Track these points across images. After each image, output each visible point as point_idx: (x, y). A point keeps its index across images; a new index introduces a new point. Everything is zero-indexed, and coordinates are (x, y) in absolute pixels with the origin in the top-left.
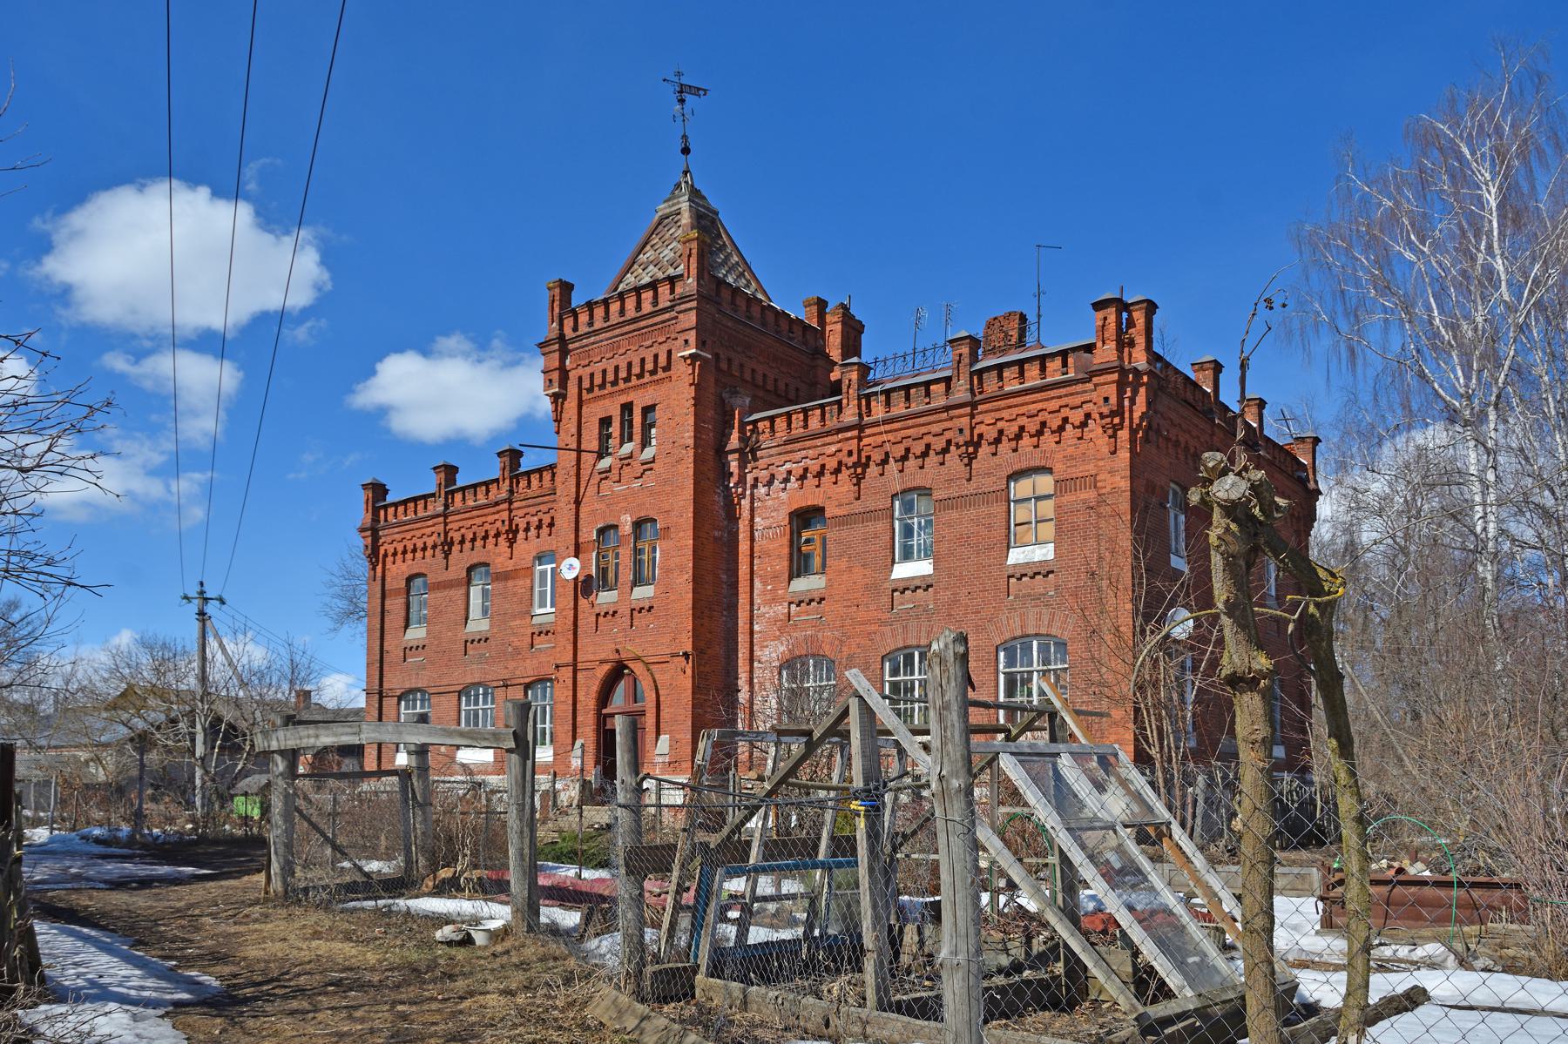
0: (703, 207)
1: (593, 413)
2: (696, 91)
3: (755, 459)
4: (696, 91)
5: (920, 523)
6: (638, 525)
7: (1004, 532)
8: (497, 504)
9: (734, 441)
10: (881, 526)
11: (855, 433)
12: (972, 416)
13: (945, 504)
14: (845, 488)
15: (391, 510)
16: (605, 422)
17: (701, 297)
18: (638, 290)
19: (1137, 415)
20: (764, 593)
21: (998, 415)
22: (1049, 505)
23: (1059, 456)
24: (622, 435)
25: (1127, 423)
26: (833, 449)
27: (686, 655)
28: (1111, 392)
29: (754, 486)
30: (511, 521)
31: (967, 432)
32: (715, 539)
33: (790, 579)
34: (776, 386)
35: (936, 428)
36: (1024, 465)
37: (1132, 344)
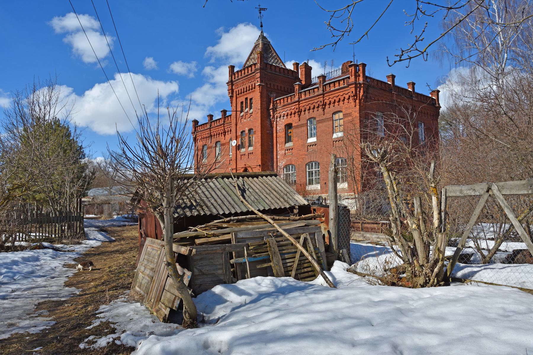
0: (266, 41)
1: (240, 100)
2: (264, 9)
3: (277, 111)
4: (264, 9)
5: (314, 127)
6: (250, 130)
7: (332, 129)
8: (221, 125)
9: (271, 107)
10: (305, 128)
11: (298, 103)
12: (323, 97)
13: (319, 122)
14: (296, 118)
15: (199, 127)
16: (242, 103)
17: (261, 69)
18: (251, 66)
19: (361, 95)
20: (280, 147)
21: (329, 97)
22: (342, 121)
23: (344, 108)
24: (246, 106)
25: (358, 98)
26: (293, 107)
27: (259, 165)
28: (353, 89)
29: (277, 118)
30: (224, 129)
31: (322, 102)
32: (267, 133)
33: (285, 143)
34: (284, 89)
35: (316, 101)
36: (336, 110)
37: (359, 76)
